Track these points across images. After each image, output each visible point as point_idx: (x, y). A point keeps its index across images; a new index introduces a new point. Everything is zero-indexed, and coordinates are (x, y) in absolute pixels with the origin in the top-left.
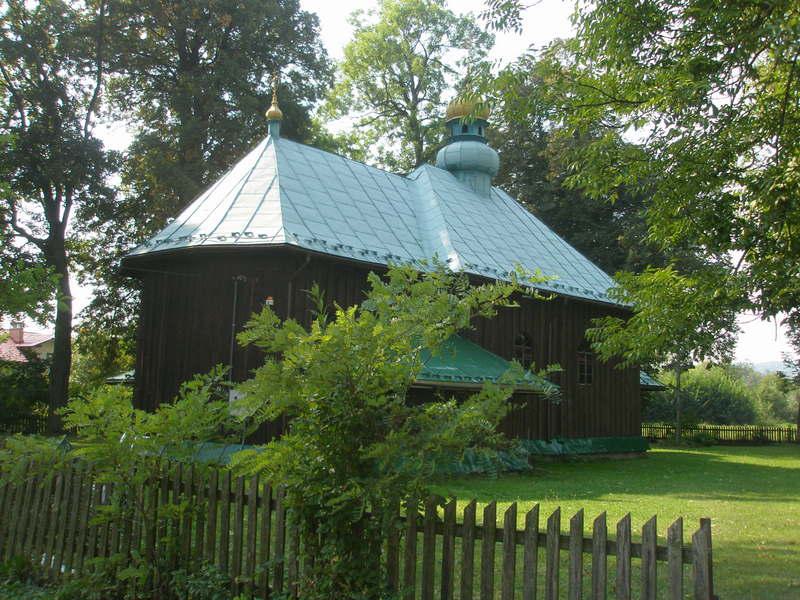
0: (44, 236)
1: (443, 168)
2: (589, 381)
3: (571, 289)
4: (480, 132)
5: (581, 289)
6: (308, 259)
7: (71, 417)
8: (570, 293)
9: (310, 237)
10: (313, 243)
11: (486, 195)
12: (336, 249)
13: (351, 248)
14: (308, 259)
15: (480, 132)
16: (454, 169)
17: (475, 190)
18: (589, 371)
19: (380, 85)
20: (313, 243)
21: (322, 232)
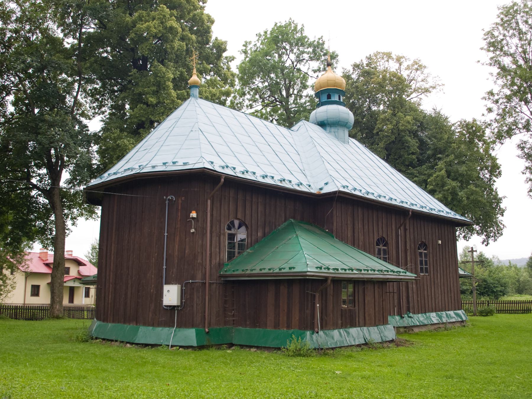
0: (51, 260)
1: (315, 124)
2: (427, 272)
3: (391, 199)
4: (340, 99)
5: (398, 200)
6: (223, 180)
7: (41, 248)
8: (390, 202)
9: (242, 169)
10: (283, 182)
11: (344, 142)
12: (243, 173)
13: (234, 168)
14: (223, 180)
15: (340, 99)
16: (322, 124)
17: (337, 138)
18: (426, 264)
19: (510, 11)
20: (283, 182)
21: (232, 162)
